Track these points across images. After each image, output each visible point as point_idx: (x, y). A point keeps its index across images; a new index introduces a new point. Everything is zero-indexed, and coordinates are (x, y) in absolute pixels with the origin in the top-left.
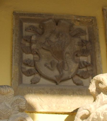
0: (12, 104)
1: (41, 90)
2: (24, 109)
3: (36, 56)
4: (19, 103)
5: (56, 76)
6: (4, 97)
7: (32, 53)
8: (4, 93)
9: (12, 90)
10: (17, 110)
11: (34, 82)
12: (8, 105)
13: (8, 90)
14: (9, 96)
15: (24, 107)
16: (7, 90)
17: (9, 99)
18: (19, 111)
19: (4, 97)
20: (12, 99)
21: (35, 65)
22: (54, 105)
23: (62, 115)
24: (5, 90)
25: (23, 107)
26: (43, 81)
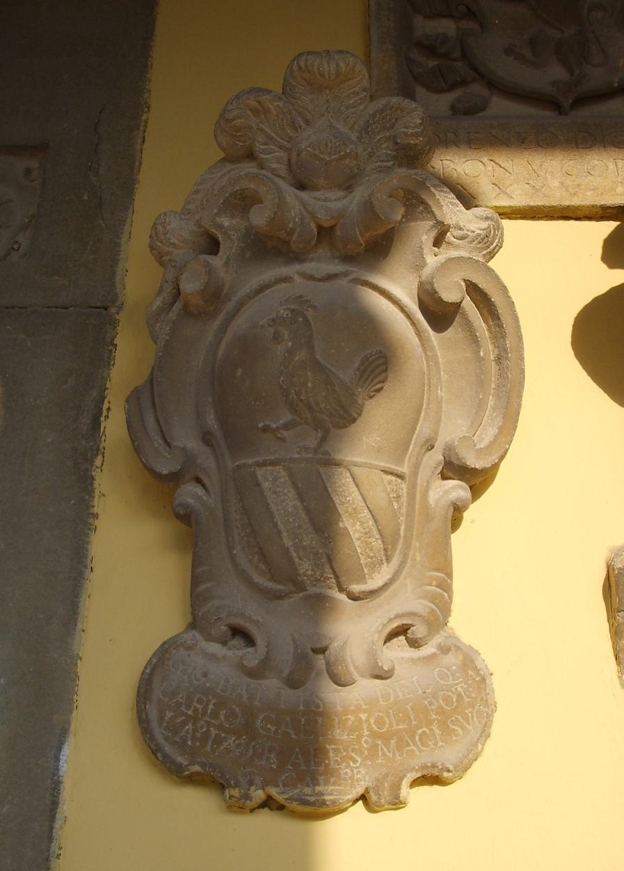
0: (366, 130)
1: (494, 132)
2: (416, 144)
3: (468, 24)
4: (392, 127)
5: (554, 84)
6: (328, 101)
7: (451, 16)
8: (323, 76)
9: (358, 68)
10: (387, 155)
11: (469, 110)
12: (342, 128)
13: (342, 65)
14: (348, 96)
15: (416, 135)
16: (337, 65)
17: (347, 108)
18: (395, 158)
19: (328, 101)
20: (361, 107)
21: (464, 55)
22: (555, 183)
23: (593, 223)
24: (328, 64)
25: (412, 135)
26: (500, 105)
